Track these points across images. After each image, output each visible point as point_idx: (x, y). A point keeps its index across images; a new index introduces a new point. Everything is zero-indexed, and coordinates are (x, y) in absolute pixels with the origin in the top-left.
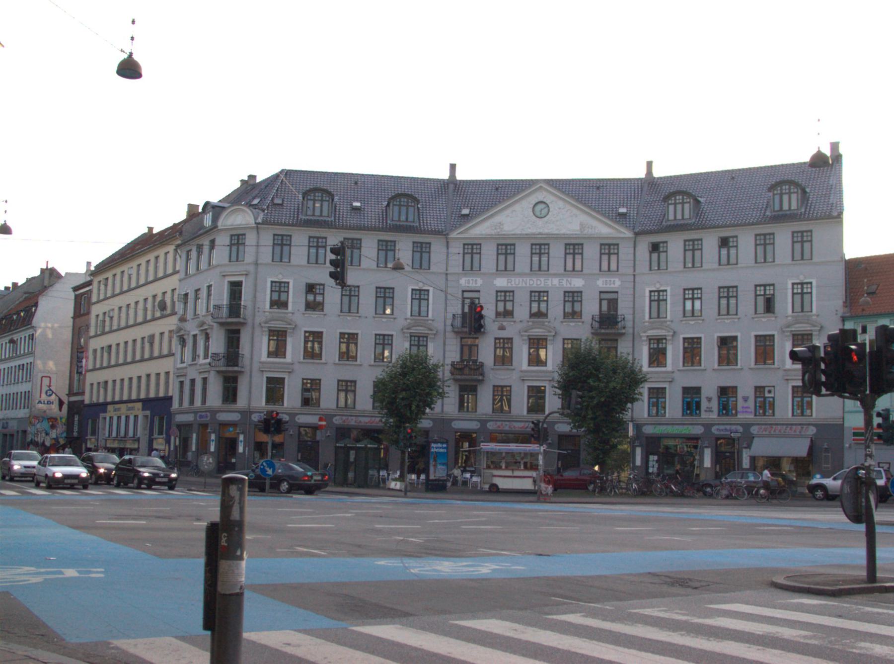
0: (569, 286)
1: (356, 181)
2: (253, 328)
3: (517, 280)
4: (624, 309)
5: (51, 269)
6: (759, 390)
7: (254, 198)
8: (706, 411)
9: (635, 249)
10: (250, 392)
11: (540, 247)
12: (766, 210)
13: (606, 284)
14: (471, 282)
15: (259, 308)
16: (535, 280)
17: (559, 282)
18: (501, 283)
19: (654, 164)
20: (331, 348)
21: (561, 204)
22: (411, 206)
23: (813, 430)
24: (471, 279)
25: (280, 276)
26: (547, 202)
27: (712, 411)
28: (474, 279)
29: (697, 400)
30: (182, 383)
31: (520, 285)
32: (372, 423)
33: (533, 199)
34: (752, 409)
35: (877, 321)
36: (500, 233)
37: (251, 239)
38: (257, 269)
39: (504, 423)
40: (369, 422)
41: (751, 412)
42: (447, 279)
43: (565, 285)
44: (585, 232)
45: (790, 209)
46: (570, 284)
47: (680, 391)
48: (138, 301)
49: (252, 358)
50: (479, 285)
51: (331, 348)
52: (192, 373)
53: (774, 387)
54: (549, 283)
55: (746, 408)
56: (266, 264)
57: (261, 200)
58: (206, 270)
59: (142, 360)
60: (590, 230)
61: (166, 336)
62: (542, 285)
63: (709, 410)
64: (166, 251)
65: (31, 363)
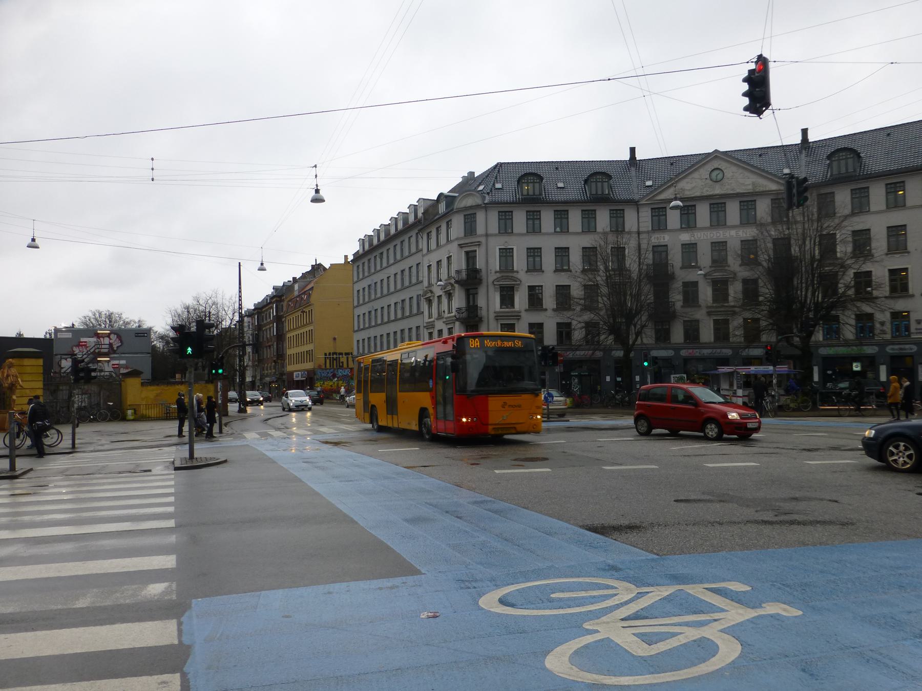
0: (745, 235)
1: (557, 166)
2: (488, 286)
3: (699, 234)
11: (718, 205)
16: (715, 233)
17: (736, 233)
18: (685, 237)
19: (809, 132)
21: (734, 169)
22: (605, 182)
26: (722, 168)
29: (906, 323)
31: (702, 238)
33: (709, 167)
36: (682, 197)
37: (480, 217)
38: (487, 240)
39: (695, 351)
45: (847, 172)
49: (488, 311)
50: (666, 240)
52: (440, 325)
54: (727, 234)
56: (495, 235)
58: (435, 250)
59: (396, 320)
61: (415, 301)
62: (722, 237)
64: (388, 248)
65: (312, 330)
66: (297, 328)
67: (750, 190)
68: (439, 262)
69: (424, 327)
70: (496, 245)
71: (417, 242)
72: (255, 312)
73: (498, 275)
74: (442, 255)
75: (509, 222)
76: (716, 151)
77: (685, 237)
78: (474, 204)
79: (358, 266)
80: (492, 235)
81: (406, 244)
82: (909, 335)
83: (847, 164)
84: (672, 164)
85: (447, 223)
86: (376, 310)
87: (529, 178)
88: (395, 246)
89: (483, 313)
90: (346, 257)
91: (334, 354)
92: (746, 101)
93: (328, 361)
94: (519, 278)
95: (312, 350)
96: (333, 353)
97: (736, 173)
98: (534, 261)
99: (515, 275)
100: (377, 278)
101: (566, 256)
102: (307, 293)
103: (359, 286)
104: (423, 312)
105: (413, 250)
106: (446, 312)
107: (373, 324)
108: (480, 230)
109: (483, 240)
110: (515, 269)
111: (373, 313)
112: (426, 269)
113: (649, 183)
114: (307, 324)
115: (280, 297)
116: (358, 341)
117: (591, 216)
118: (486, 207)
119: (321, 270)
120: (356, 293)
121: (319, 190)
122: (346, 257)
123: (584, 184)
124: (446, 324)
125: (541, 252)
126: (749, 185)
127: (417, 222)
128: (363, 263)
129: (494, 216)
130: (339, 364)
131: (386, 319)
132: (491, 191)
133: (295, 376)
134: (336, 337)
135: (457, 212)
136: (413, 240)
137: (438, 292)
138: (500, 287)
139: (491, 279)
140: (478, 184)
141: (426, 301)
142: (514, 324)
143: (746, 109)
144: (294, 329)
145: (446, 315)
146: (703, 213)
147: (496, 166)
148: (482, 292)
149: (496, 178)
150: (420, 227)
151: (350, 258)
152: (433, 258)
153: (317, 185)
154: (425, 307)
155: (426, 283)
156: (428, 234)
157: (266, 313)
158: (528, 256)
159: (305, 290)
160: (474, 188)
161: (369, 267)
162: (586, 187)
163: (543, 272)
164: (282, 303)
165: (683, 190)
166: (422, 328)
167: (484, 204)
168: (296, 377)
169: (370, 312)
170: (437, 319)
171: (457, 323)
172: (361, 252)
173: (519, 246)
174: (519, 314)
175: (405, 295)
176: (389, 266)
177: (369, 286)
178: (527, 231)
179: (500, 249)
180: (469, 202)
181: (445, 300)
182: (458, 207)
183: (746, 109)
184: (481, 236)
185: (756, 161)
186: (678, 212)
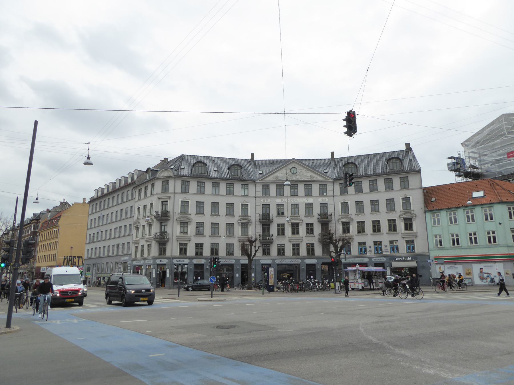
1: (214, 159)
2: (173, 221)
3: (285, 199)
4: (330, 210)
5: (65, 202)
6: (391, 242)
7: (172, 165)
8: (369, 252)
9: (333, 186)
10: (172, 250)
12: (387, 169)
13: (265, 201)
14: (266, 200)
15: (176, 212)
16: (293, 199)
18: (279, 201)
20: (207, 230)
21: (302, 168)
23: (188, 261)
24: (265, 199)
25: (185, 199)
27: (372, 252)
28: (267, 199)
30: (136, 247)
32: (226, 262)
33: (290, 166)
34: (389, 250)
35: (493, 206)
37: (171, 183)
38: (174, 196)
39: (283, 260)
40: (225, 262)
41: (389, 252)
42: (255, 200)
43: (305, 201)
44: (312, 179)
46: (308, 201)
47: (357, 244)
48: (92, 219)
50: (269, 202)
51: (207, 230)
52: (143, 242)
53: (398, 241)
54: (299, 200)
55: (387, 250)
56: (180, 193)
57: (175, 167)
59: (115, 238)
60: (314, 179)
62: (296, 201)
63: (370, 251)
65: (57, 241)
66: (46, 240)
67: (309, 179)
68: (145, 207)
69: (133, 243)
70: (179, 198)
71: (132, 194)
72: (18, 228)
73: (180, 215)
74: (147, 202)
75: (187, 187)
76: (293, 159)
77: (279, 201)
78: (168, 176)
79: (93, 205)
80: (177, 193)
81: (125, 194)
82: (382, 253)
83: (396, 165)
84: (272, 163)
85: (152, 184)
86: (102, 232)
87: (199, 164)
88: (118, 195)
89: (170, 236)
90: (84, 199)
91: (70, 257)
92: (345, 130)
93: (66, 261)
94: (191, 217)
95: (56, 254)
96: (69, 256)
97: (303, 170)
98: (295, 210)
99: (189, 216)
100: (105, 213)
101: (297, 208)
102: (56, 219)
103: (92, 217)
104: (132, 234)
105: (130, 198)
106: (148, 235)
107: (99, 239)
108: (171, 189)
109: (172, 195)
110: (189, 213)
111: (100, 233)
112: (136, 210)
113: (261, 172)
114: (54, 238)
115: (38, 220)
116: (88, 250)
117: (231, 186)
118: (175, 177)
119: (66, 206)
120: (89, 221)
121: (90, 157)
122: (84, 199)
123: (228, 170)
124: (147, 242)
125: (204, 204)
126: (309, 176)
127: (133, 183)
128: (97, 204)
129: (179, 183)
130: (73, 263)
131: (108, 237)
132: (178, 169)
133: (41, 269)
134: (73, 246)
135: (158, 179)
136: (130, 193)
137: (143, 222)
138: (342, 223)
139: (175, 218)
140: (171, 165)
141: (135, 228)
142: (187, 243)
143: (345, 133)
144: (44, 240)
145: (147, 236)
146: (301, 189)
147: (181, 156)
148: (170, 223)
149: (181, 163)
150: (135, 186)
151: (87, 200)
152: (141, 204)
153: (89, 155)
154: (134, 231)
155: (136, 217)
156: (140, 190)
157: (26, 229)
158: (197, 206)
159: (55, 217)
160: (168, 167)
161: (100, 206)
162: (229, 171)
163: (234, 216)
164: (38, 224)
165: (277, 177)
166: (131, 244)
167: (174, 176)
168: (42, 270)
169: (98, 233)
170: (141, 239)
171: (154, 242)
172: (96, 197)
173: (192, 200)
174: (190, 238)
175: (122, 224)
176: (113, 206)
177: (99, 217)
178: (181, 191)
179: (181, 201)
180: (166, 174)
181: (147, 228)
182: (159, 176)
183: (345, 133)
184: (171, 193)
185: (311, 165)
186: (289, 187)
